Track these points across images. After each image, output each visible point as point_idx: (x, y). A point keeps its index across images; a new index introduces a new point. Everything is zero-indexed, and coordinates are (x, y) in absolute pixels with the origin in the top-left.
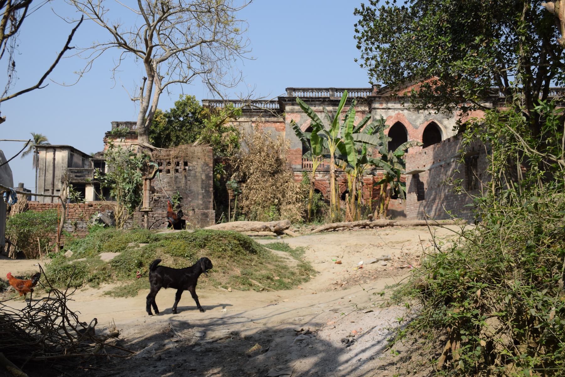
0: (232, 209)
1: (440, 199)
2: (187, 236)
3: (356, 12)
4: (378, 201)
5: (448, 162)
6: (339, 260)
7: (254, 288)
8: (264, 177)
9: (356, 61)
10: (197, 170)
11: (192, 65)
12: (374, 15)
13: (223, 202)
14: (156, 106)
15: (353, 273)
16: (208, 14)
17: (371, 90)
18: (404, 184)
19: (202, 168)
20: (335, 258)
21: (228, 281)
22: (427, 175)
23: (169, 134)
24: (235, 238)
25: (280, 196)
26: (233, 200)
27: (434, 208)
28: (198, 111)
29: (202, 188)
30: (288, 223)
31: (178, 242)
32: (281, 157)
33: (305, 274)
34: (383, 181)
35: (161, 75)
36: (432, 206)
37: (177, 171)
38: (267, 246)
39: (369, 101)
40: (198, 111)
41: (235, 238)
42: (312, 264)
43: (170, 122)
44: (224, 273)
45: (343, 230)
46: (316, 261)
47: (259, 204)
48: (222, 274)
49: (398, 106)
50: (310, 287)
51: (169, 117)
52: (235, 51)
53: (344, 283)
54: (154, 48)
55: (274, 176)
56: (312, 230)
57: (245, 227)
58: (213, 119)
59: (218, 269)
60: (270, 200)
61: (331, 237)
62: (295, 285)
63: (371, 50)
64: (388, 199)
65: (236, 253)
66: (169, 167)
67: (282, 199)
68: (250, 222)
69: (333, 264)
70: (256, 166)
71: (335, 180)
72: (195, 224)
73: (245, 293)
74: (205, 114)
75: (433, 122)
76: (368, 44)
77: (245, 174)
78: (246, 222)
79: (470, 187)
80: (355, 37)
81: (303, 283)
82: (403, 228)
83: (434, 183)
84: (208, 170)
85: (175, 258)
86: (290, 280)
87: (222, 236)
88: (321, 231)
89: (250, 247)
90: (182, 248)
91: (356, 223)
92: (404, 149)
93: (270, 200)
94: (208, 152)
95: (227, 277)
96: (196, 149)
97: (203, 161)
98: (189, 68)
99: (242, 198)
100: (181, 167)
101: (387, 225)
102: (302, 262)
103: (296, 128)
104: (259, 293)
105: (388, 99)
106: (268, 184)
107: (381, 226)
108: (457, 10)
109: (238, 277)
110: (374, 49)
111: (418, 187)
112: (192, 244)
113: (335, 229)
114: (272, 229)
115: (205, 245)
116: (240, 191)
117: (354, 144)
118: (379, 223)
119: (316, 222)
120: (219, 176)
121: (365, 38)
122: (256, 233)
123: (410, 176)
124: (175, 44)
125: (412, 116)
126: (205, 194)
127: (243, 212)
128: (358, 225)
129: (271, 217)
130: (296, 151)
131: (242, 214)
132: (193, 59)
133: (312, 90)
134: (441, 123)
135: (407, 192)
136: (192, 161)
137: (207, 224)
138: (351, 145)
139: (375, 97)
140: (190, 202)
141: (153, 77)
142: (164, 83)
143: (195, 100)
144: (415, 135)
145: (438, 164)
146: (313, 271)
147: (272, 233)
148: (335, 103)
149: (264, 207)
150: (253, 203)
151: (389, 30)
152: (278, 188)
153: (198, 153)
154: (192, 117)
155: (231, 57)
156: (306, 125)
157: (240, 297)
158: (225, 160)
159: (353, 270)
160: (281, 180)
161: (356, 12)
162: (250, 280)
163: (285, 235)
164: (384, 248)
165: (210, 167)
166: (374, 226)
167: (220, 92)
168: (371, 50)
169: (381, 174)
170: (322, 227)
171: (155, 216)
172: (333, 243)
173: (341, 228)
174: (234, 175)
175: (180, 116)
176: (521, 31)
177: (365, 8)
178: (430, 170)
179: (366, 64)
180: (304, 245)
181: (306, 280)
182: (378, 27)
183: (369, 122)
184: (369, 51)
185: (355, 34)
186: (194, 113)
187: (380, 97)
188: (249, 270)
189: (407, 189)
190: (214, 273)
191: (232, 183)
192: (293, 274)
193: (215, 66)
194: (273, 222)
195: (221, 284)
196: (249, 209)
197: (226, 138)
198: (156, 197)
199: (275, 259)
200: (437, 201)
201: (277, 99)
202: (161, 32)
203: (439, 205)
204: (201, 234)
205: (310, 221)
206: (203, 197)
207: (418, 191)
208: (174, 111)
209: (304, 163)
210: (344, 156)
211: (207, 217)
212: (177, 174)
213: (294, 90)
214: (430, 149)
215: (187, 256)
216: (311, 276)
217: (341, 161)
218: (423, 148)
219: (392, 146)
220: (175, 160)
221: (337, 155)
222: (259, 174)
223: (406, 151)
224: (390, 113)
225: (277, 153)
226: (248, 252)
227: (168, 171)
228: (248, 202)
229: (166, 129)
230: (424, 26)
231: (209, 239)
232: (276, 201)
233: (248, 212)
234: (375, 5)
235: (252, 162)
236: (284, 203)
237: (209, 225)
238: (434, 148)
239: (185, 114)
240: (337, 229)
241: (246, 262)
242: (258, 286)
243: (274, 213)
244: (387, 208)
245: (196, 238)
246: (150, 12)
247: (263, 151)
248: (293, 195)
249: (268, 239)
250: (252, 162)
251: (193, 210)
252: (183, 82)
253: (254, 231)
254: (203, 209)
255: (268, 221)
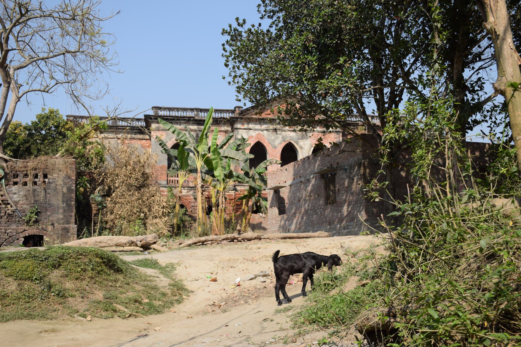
0: (95, 224)
1: (300, 213)
2: (37, 255)
3: (224, 32)
4: (242, 215)
5: (308, 178)
6: (214, 277)
7: (119, 314)
8: (130, 191)
9: (224, 78)
10: (58, 183)
11: (54, 75)
12: (241, 35)
13: (85, 217)
14: (13, 115)
15: (230, 291)
16: (73, 22)
17: (233, 112)
18: (266, 199)
19: (63, 181)
20: (209, 275)
21: (87, 307)
22: (288, 190)
23: (29, 147)
24: (97, 255)
25: (146, 210)
26: (97, 214)
27: (295, 221)
28: (61, 125)
29: (63, 202)
30: (155, 238)
31: (25, 262)
32: (147, 171)
33: (177, 294)
34: (245, 197)
35: (19, 82)
36: (293, 220)
37: (35, 183)
38: (134, 263)
39: (231, 122)
40: (61, 125)
41: (97, 255)
42: (185, 283)
43: (31, 135)
44: (82, 297)
45: (212, 244)
46: (189, 279)
47: (124, 219)
48: (80, 300)
49: (258, 127)
50: (184, 310)
51: (29, 130)
52: (101, 63)
53: (222, 304)
54: (10, 52)
55: (140, 190)
56: (180, 244)
57: (109, 242)
58: (77, 131)
59: (75, 293)
60: (135, 214)
61: (201, 251)
62: (167, 307)
63: (238, 68)
64: (250, 213)
65: (98, 273)
66: (26, 180)
67: (148, 213)
68: (114, 237)
69: (208, 282)
70: (122, 180)
71: (202, 193)
72: (54, 240)
73: (108, 322)
74: (69, 128)
75: (290, 142)
76: (235, 62)
77: (110, 188)
78: (110, 237)
79: (329, 202)
80: (222, 55)
81: (176, 305)
82: (273, 241)
83: (295, 198)
84: (70, 183)
85: (20, 282)
86: (160, 303)
87: (81, 253)
88: (189, 245)
89: (115, 266)
90: (30, 269)
91: (225, 236)
92: (265, 166)
93: (135, 214)
94: (70, 164)
95: (86, 302)
96: (57, 161)
97: (65, 173)
98: (52, 78)
99: (107, 212)
100: (40, 179)
101: (255, 238)
102: (174, 280)
103: (162, 144)
104: (125, 320)
105: (250, 120)
106: (134, 198)
107: (249, 240)
108: (322, 32)
109: (99, 302)
110: (241, 67)
111: (279, 202)
112: (44, 264)
113: (203, 243)
114: (139, 244)
115: (60, 265)
116: (105, 205)
117: (221, 160)
118: (247, 237)
119: (183, 236)
120: (82, 189)
121: (233, 56)
122: (121, 249)
123: (272, 192)
124: (36, 52)
125: (271, 137)
126: (66, 208)
127: (108, 227)
128: (227, 239)
129: (137, 232)
130: (162, 168)
131: (106, 228)
132: (56, 69)
133: (178, 109)
134: (297, 144)
135: (268, 207)
136: (53, 173)
137: (68, 239)
138: (218, 160)
139: (237, 118)
140: (49, 216)
141: (9, 83)
142: (22, 90)
143: (58, 114)
144: (274, 153)
145: (298, 180)
146: (186, 290)
147: (138, 248)
148: (200, 122)
149: (129, 221)
150: (118, 217)
151: (256, 50)
152: (144, 202)
153: (60, 166)
154: (55, 131)
155: (97, 69)
156: (171, 142)
157: (102, 327)
158: (89, 173)
159: (230, 289)
160: (147, 194)
161: (224, 32)
162: (115, 305)
163: (152, 250)
164: (259, 263)
165: (72, 180)
166: (243, 239)
167: (84, 104)
168: (238, 68)
169: (244, 189)
170: (190, 242)
171: (8, 231)
172: (205, 258)
173: (210, 242)
174: (98, 189)
175: (42, 129)
176: (436, 17)
177: (233, 29)
178: (290, 186)
179: (233, 81)
180: (175, 261)
181: (179, 302)
182: (244, 47)
183: (231, 141)
184: (236, 69)
185: (223, 52)
186: (57, 127)
187: (241, 118)
188: (113, 293)
189: (268, 204)
190: (70, 299)
191: (96, 196)
192: (164, 295)
193: (79, 77)
194: (139, 236)
195: (78, 312)
196: (114, 223)
197: (91, 151)
198: (9, 211)
199: (143, 279)
200: (297, 215)
201: (143, 117)
202: (19, 39)
203: (300, 219)
204: (56, 252)
205: (176, 235)
206: (64, 211)
207: (279, 206)
208: (35, 124)
209: (169, 179)
210: (210, 172)
211: (68, 232)
212: (36, 187)
213: (160, 108)
214: (290, 166)
215: (36, 279)
216: (184, 297)
217: (207, 176)
218: (281, 166)
219: (254, 163)
220: (33, 172)
221: (204, 171)
222: (124, 188)
223: (266, 168)
224: (251, 133)
225: (143, 166)
226: (112, 271)
227: (25, 184)
228: (112, 217)
229: (26, 141)
230: (290, 45)
231: (65, 258)
232: (142, 215)
233: (112, 226)
234: (242, 26)
235: (117, 176)
236: (151, 218)
237: (70, 241)
238: (295, 166)
239: (48, 127)
240: (205, 243)
241: (110, 284)
242: (124, 312)
243: (140, 227)
244: (249, 222)
245: (49, 257)
246: (7, 16)
247: (129, 165)
248: (160, 209)
249: (134, 254)
250: (117, 176)
251: (53, 224)
252: (44, 91)
253: (119, 246)
254: (63, 224)
255: (133, 235)
